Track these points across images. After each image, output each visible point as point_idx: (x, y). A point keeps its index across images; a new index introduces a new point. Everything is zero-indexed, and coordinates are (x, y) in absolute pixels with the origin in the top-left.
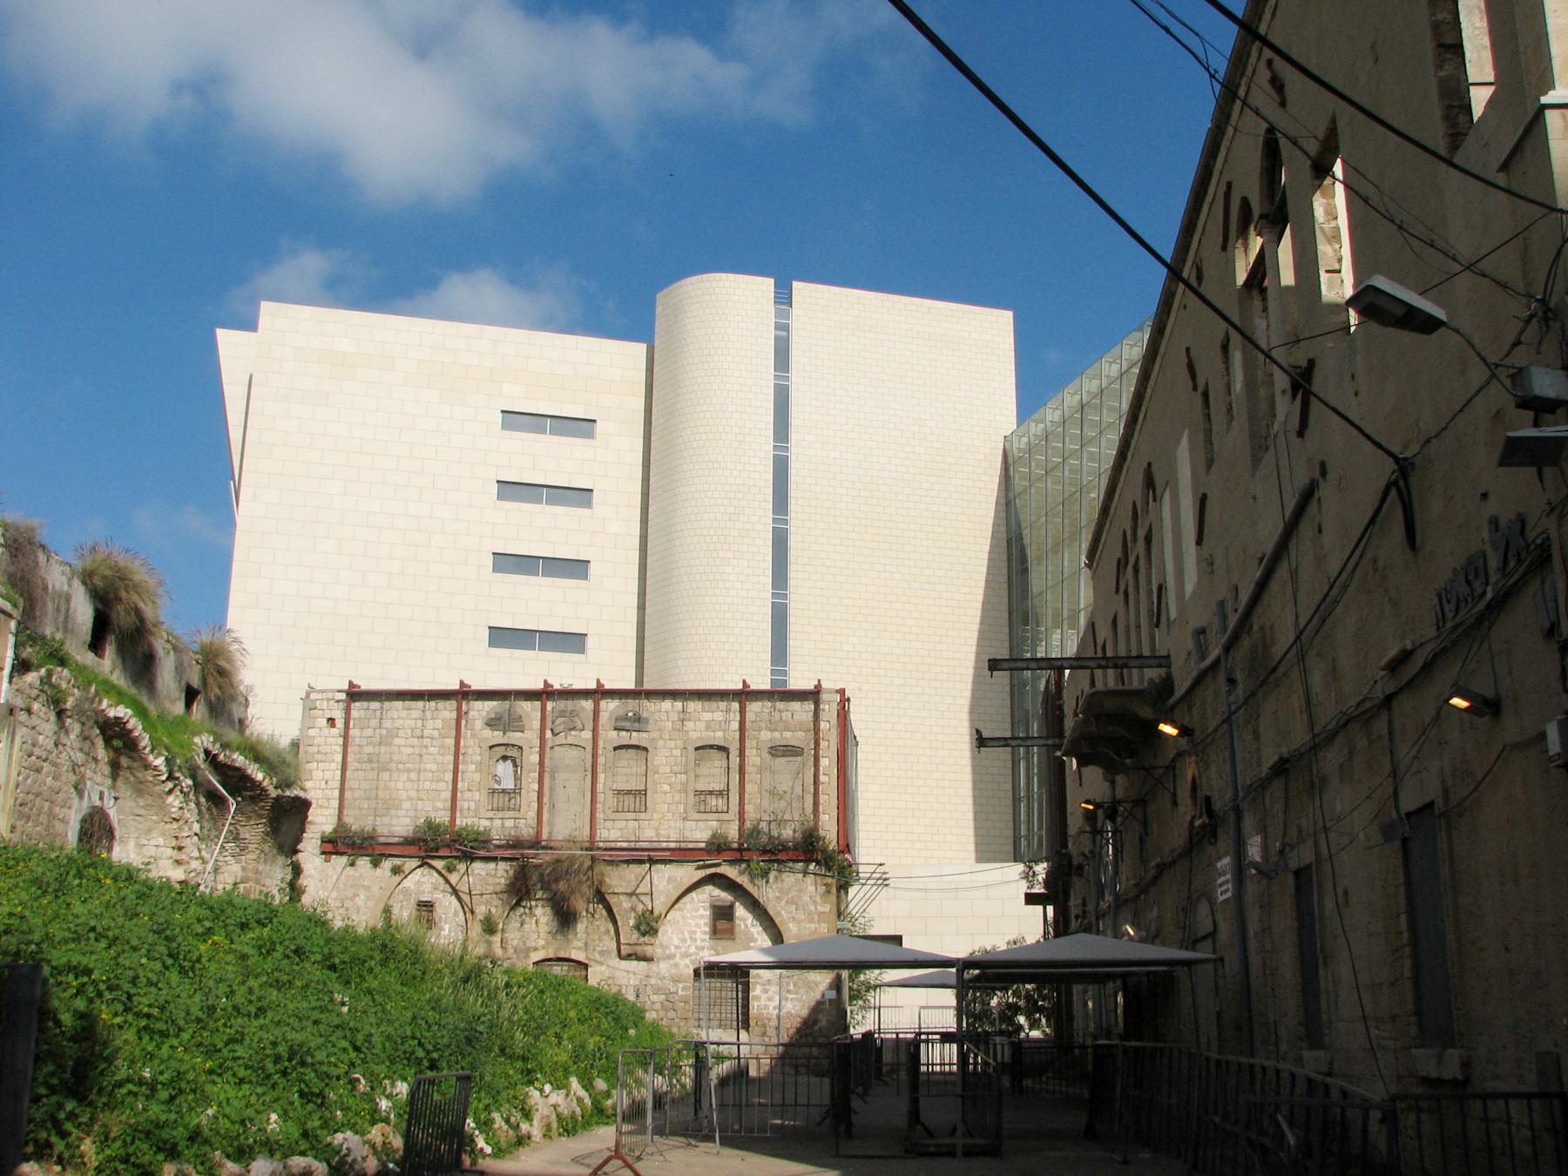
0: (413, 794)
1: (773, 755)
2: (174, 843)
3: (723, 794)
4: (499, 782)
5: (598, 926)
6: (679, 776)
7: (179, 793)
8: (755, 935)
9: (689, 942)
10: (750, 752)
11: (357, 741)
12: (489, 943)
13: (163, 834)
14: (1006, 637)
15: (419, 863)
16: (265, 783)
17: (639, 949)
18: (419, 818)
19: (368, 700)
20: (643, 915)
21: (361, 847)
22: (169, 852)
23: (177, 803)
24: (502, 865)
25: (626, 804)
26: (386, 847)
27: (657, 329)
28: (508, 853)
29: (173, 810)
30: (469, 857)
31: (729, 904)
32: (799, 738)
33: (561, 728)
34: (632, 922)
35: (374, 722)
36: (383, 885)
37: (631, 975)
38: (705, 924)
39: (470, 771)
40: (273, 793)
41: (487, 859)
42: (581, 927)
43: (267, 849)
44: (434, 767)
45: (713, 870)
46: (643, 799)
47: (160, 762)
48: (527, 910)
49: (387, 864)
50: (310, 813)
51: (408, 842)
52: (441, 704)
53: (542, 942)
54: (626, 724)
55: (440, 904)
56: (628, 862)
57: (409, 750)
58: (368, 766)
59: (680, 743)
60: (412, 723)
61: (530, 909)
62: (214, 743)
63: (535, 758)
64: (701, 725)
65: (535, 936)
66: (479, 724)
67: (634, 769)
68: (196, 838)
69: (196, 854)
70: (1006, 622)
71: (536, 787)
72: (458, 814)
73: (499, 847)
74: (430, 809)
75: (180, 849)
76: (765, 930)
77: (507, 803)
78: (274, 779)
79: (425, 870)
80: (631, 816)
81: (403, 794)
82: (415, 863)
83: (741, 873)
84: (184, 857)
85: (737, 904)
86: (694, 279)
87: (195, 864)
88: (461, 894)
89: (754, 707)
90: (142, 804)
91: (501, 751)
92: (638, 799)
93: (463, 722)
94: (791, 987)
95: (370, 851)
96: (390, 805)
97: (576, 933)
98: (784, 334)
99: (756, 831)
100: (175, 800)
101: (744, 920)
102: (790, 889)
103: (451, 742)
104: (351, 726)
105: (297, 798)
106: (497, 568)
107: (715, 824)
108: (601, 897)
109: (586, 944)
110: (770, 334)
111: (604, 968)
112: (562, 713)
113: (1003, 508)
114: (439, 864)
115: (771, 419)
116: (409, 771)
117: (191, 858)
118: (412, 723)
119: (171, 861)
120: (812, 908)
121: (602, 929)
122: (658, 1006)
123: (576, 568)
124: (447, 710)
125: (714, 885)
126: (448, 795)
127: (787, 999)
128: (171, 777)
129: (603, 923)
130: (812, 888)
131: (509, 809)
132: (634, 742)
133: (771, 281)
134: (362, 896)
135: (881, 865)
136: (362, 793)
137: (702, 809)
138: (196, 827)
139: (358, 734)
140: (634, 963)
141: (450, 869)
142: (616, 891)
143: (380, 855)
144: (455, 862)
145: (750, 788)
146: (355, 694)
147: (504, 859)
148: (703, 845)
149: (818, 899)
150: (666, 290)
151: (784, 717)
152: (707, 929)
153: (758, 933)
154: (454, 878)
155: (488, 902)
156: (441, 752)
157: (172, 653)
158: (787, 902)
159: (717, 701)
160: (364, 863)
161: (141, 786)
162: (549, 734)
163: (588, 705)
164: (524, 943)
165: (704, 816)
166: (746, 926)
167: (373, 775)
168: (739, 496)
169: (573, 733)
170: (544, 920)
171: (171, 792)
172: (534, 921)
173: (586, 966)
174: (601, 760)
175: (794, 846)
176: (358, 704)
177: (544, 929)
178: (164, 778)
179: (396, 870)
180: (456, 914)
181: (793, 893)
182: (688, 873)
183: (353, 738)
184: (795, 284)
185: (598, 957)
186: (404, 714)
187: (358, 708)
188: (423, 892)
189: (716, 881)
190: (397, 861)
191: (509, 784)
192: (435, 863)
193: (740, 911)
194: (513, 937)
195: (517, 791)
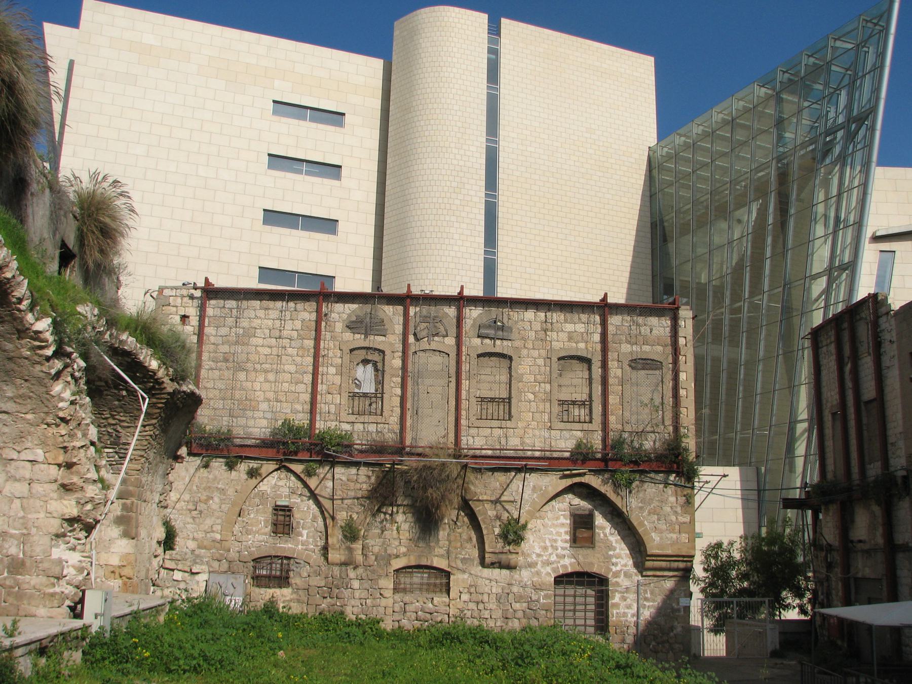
0: (271, 395)
1: (633, 368)
2: (61, 459)
3: (587, 404)
4: (359, 386)
5: (460, 534)
6: (542, 385)
7: (69, 379)
8: (614, 544)
9: (550, 550)
10: (612, 365)
11: (212, 339)
12: (350, 550)
13: (43, 443)
14: (650, 294)
15: (278, 466)
16: (161, 373)
17: (503, 558)
18: (276, 420)
19: (224, 299)
20: (509, 524)
21: (217, 448)
22: (54, 471)
23: (67, 395)
24: (363, 470)
25: (490, 411)
26: (244, 449)
27: (395, 48)
28: (372, 459)
29: (61, 405)
30: (333, 462)
31: (587, 512)
32: (659, 352)
33: (424, 333)
34: (497, 531)
35: (230, 321)
36: (239, 488)
37: (494, 583)
38: (566, 533)
39: (330, 373)
40: (170, 387)
41: (348, 464)
42: (443, 534)
43: (151, 455)
44: (292, 368)
45: (577, 480)
46: (507, 407)
47: (44, 325)
48: (388, 516)
49: (243, 467)
50: (199, 411)
51: (265, 444)
52: (300, 305)
53: (403, 549)
54: (491, 332)
55: (298, 508)
56: (494, 470)
57: (267, 351)
58: (223, 365)
59: (543, 353)
60: (270, 323)
61: (391, 515)
62: (100, 316)
63: (398, 363)
64: (563, 336)
65: (397, 543)
66: (339, 327)
67: (497, 377)
68: (92, 449)
69: (93, 475)
70: (650, 283)
71: (398, 391)
72: (318, 418)
73: (361, 452)
74: (289, 411)
75: (69, 466)
76: (623, 539)
77: (367, 407)
78: (171, 370)
79: (283, 474)
80: (495, 423)
81: (260, 395)
82: (272, 466)
83: (605, 482)
84: (75, 479)
85: (596, 513)
86: (427, 10)
87: (92, 491)
88: (320, 499)
89: (615, 321)
90: (10, 394)
91: (362, 354)
92: (501, 407)
93: (323, 324)
94: (648, 595)
95: (225, 453)
96: (248, 405)
97: (438, 540)
98: (493, 57)
99: (619, 443)
100: (64, 389)
101: (603, 528)
102: (651, 500)
103: (310, 343)
104: (206, 324)
105: (193, 394)
106: (266, 221)
107: (579, 434)
108: (466, 507)
109: (448, 552)
110: (485, 56)
111: (466, 576)
112: (425, 319)
113: (648, 199)
114: (298, 468)
115: (485, 118)
116: (266, 371)
117: (86, 481)
118: (270, 323)
119: (55, 486)
120: (673, 518)
121: (465, 536)
122: (520, 614)
123: (328, 225)
124: (306, 312)
125: (574, 494)
126: (307, 397)
127: (644, 607)
128: (59, 353)
129: (465, 531)
130: (672, 499)
131: (370, 414)
132: (498, 350)
133: (486, 16)
134: (216, 500)
135: (725, 476)
136: (217, 392)
137: (565, 419)
138: (93, 432)
139: (214, 333)
140: (497, 571)
141: (310, 474)
142: (480, 498)
143: (236, 457)
144: (315, 466)
145: (613, 399)
146: (210, 292)
147: (367, 464)
148: (567, 455)
149: (679, 509)
150: (402, 19)
151: (643, 331)
152: (568, 537)
153: (616, 542)
154: (313, 483)
155: (349, 508)
156: (300, 353)
157: (47, 191)
158: (649, 513)
159: (578, 313)
160: (218, 465)
161: (10, 366)
162: (411, 339)
163: (451, 311)
164: (386, 550)
165: (569, 426)
166: (605, 535)
167: (227, 374)
168: (461, 174)
169: (436, 338)
170: (405, 526)
171: (58, 375)
172: (395, 528)
173: (448, 574)
174: (465, 367)
175: (656, 457)
176: (213, 302)
177: (405, 535)
178: (49, 352)
179: (252, 473)
180: (314, 519)
181: (655, 504)
182: (552, 482)
183: (208, 336)
184: (503, 20)
185: (460, 565)
186: (261, 313)
187: (213, 307)
188: (280, 496)
189: (576, 490)
190: (254, 464)
191: (369, 387)
192: (293, 467)
193: (599, 520)
194: (375, 544)
195: (379, 395)
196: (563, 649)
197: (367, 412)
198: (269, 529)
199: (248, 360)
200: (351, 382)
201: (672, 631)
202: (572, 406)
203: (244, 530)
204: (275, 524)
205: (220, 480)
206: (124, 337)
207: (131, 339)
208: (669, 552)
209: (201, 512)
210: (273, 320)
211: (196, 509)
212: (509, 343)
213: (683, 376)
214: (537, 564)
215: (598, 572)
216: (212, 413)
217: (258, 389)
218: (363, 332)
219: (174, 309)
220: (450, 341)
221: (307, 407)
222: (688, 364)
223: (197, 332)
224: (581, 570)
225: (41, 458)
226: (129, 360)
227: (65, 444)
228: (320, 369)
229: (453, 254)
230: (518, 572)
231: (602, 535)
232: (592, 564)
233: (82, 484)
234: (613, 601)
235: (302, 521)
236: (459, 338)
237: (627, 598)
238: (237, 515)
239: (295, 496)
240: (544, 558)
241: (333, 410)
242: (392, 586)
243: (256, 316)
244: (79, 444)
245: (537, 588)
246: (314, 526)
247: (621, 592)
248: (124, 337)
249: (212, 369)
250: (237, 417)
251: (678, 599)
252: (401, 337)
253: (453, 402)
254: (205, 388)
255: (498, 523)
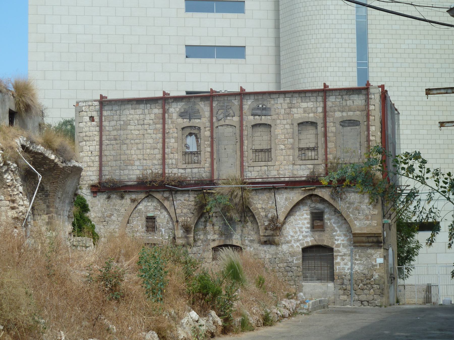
0: (140, 157)
9: (299, 233)
25: (260, 157)
29: (8, 181)
32: (356, 115)
36: (127, 208)
38: (308, 223)
39: (171, 142)
44: (151, 141)
45: (311, 193)
54: (259, 112)
55: (159, 217)
57: (137, 132)
59: (289, 121)
60: (137, 117)
63: (208, 133)
64: (301, 111)
66: (175, 116)
68: (21, 194)
71: (209, 149)
80: (263, 164)
84: (15, 205)
91: (188, 131)
93: (166, 115)
94: (357, 257)
96: (129, 163)
100: (8, 176)
103: (160, 126)
105: (74, 167)
107: (311, 167)
116: (137, 144)
117: (19, 205)
126: (159, 156)
127: (355, 264)
137: (303, 158)
139: (108, 125)
152: (309, 226)
156: (155, 132)
162: (215, 119)
169: (228, 118)
174: (245, 133)
180: (168, 223)
183: (105, 127)
191: (193, 148)
195: (197, 153)
196: (12, 216)
197: (193, 162)
198: (144, 229)
199: (127, 139)
200: (183, 146)
201: (373, 277)
202: (307, 151)
203: (131, 231)
204: (147, 227)
205: (116, 204)
206: (38, 147)
207: (42, 147)
208: (365, 231)
209: (108, 223)
210: (139, 115)
211: (105, 221)
212: (269, 117)
213: (372, 129)
214: (291, 241)
215: (327, 244)
216: (110, 169)
217: (134, 153)
218: (188, 117)
219: (86, 113)
220: (236, 119)
221: (160, 162)
222: (376, 121)
223: (98, 125)
224: (317, 244)
225: (3, 199)
226: (42, 156)
227: (11, 194)
228: (166, 140)
229: (330, 22)
230: (281, 246)
231: (329, 224)
232: (323, 240)
233: (18, 206)
234: (336, 261)
235: (161, 224)
236: (241, 116)
237: (345, 259)
238: (126, 222)
239: (157, 211)
240: (296, 238)
241: (174, 162)
242: (211, 256)
243: (130, 113)
244: (15, 193)
245: (292, 255)
246: (168, 226)
247: (341, 256)
248: (38, 147)
249: (108, 145)
250: (123, 170)
251: (375, 259)
252: (209, 119)
253: (239, 153)
254: (106, 155)
255: (266, 219)
